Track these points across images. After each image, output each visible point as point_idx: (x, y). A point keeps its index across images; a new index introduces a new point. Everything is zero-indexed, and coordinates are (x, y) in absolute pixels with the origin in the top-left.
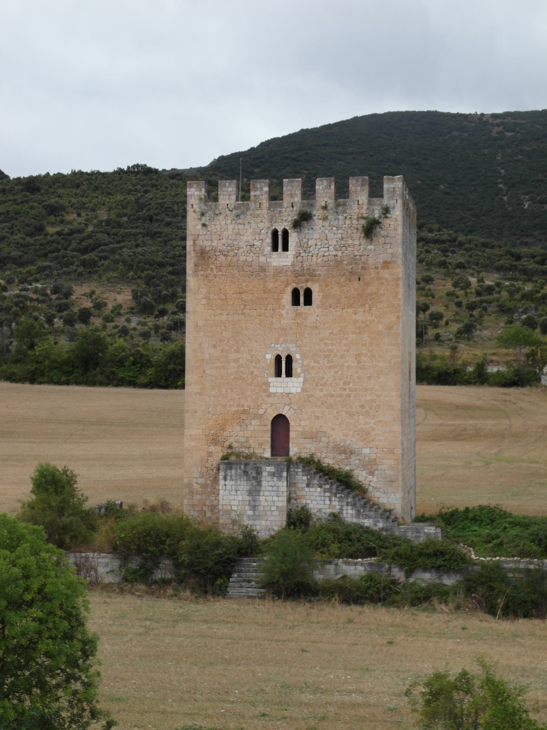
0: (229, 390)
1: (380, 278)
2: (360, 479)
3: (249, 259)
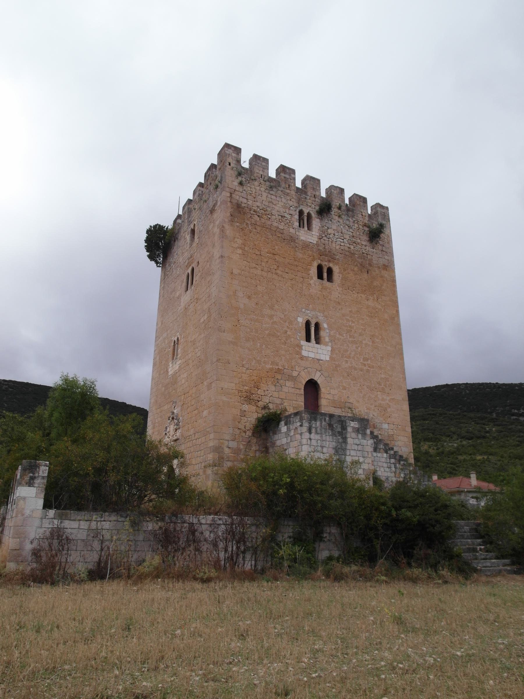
0: (264, 346)
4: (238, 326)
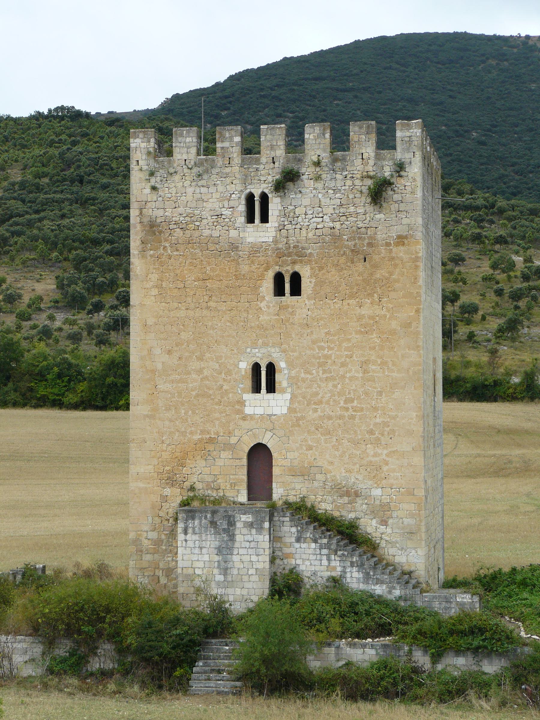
1: (393, 258)
2: (369, 530)
3: (216, 234)
4: (155, 393)
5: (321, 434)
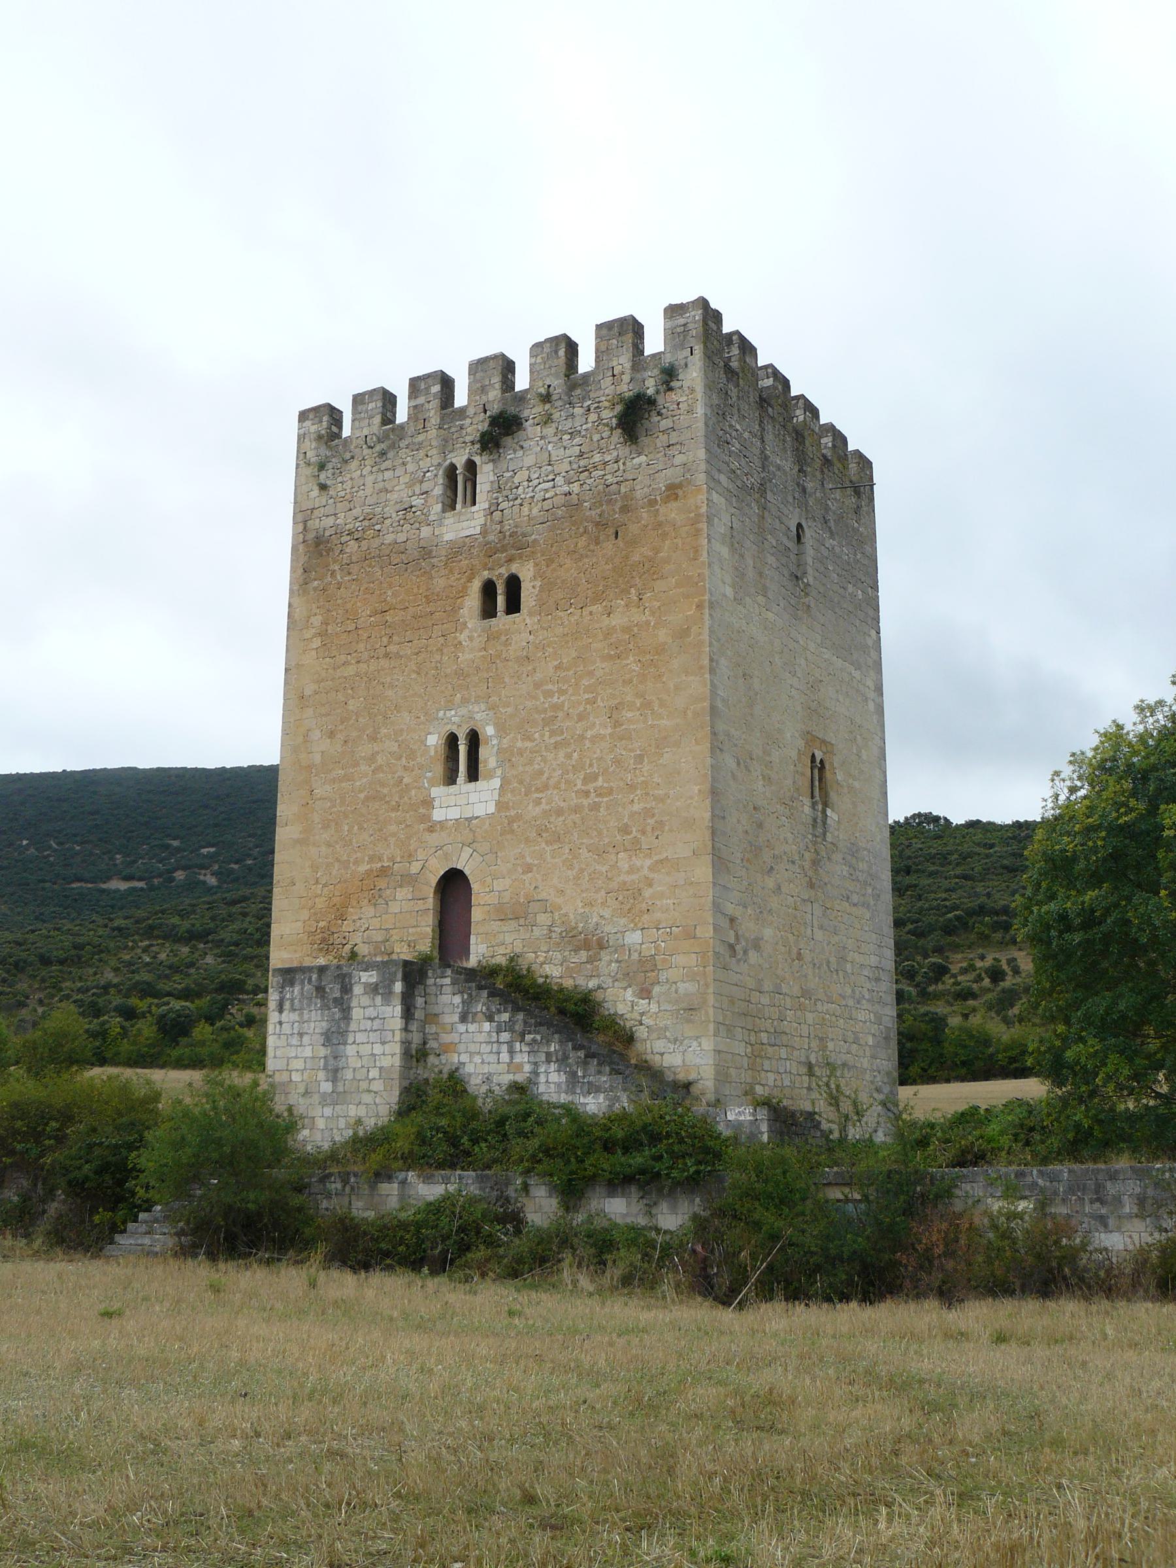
1: (660, 524)
2: (621, 1009)
3: (401, 537)
5: (547, 843)
